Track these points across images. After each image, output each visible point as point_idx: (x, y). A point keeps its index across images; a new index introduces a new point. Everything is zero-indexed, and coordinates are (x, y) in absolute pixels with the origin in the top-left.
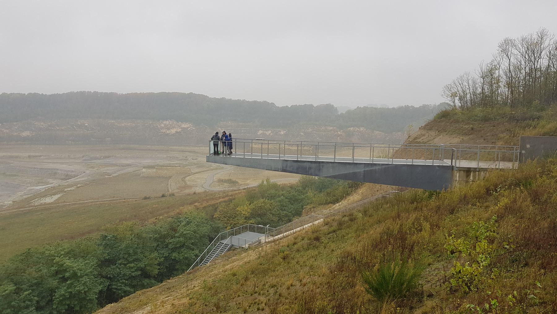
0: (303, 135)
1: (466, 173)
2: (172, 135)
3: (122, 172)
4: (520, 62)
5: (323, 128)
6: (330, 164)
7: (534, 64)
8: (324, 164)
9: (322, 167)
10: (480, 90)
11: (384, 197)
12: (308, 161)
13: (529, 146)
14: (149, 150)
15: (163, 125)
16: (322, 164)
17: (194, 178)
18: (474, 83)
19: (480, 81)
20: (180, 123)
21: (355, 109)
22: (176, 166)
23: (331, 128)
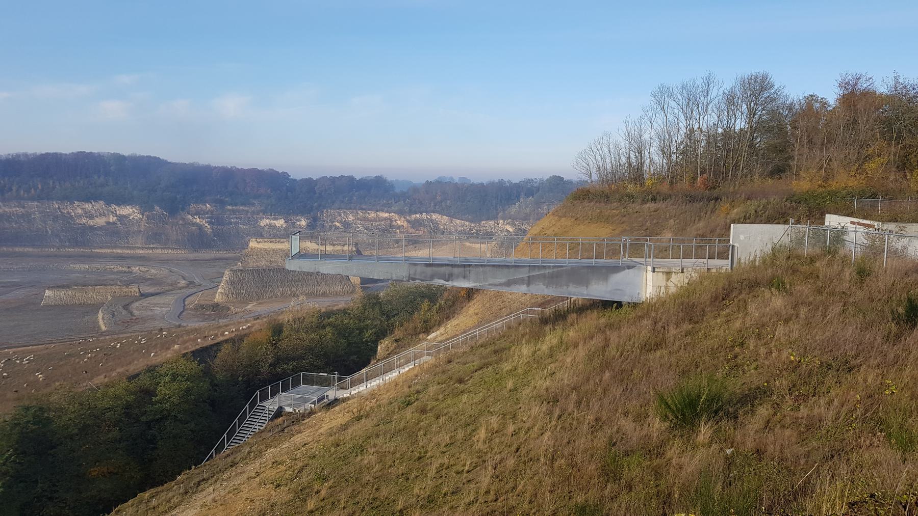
0: (340, 226)
1: (666, 275)
2: (101, 228)
3: (4, 298)
4: (678, 119)
5: (373, 215)
6: (480, 267)
7: (699, 123)
8: (471, 268)
9: (468, 273)
10: (624, 160)
11: (220, 350)
12: (658, 258)
13: (743, 238)
14: (56, 256)
15: (80, 211)
16: (468, 269)
17: (148, 303)
18: (617, 146)
19: (624, 144)
20: (114, 206)
21: (446, 183)
22: (112, 284)
23: (386, 215)
